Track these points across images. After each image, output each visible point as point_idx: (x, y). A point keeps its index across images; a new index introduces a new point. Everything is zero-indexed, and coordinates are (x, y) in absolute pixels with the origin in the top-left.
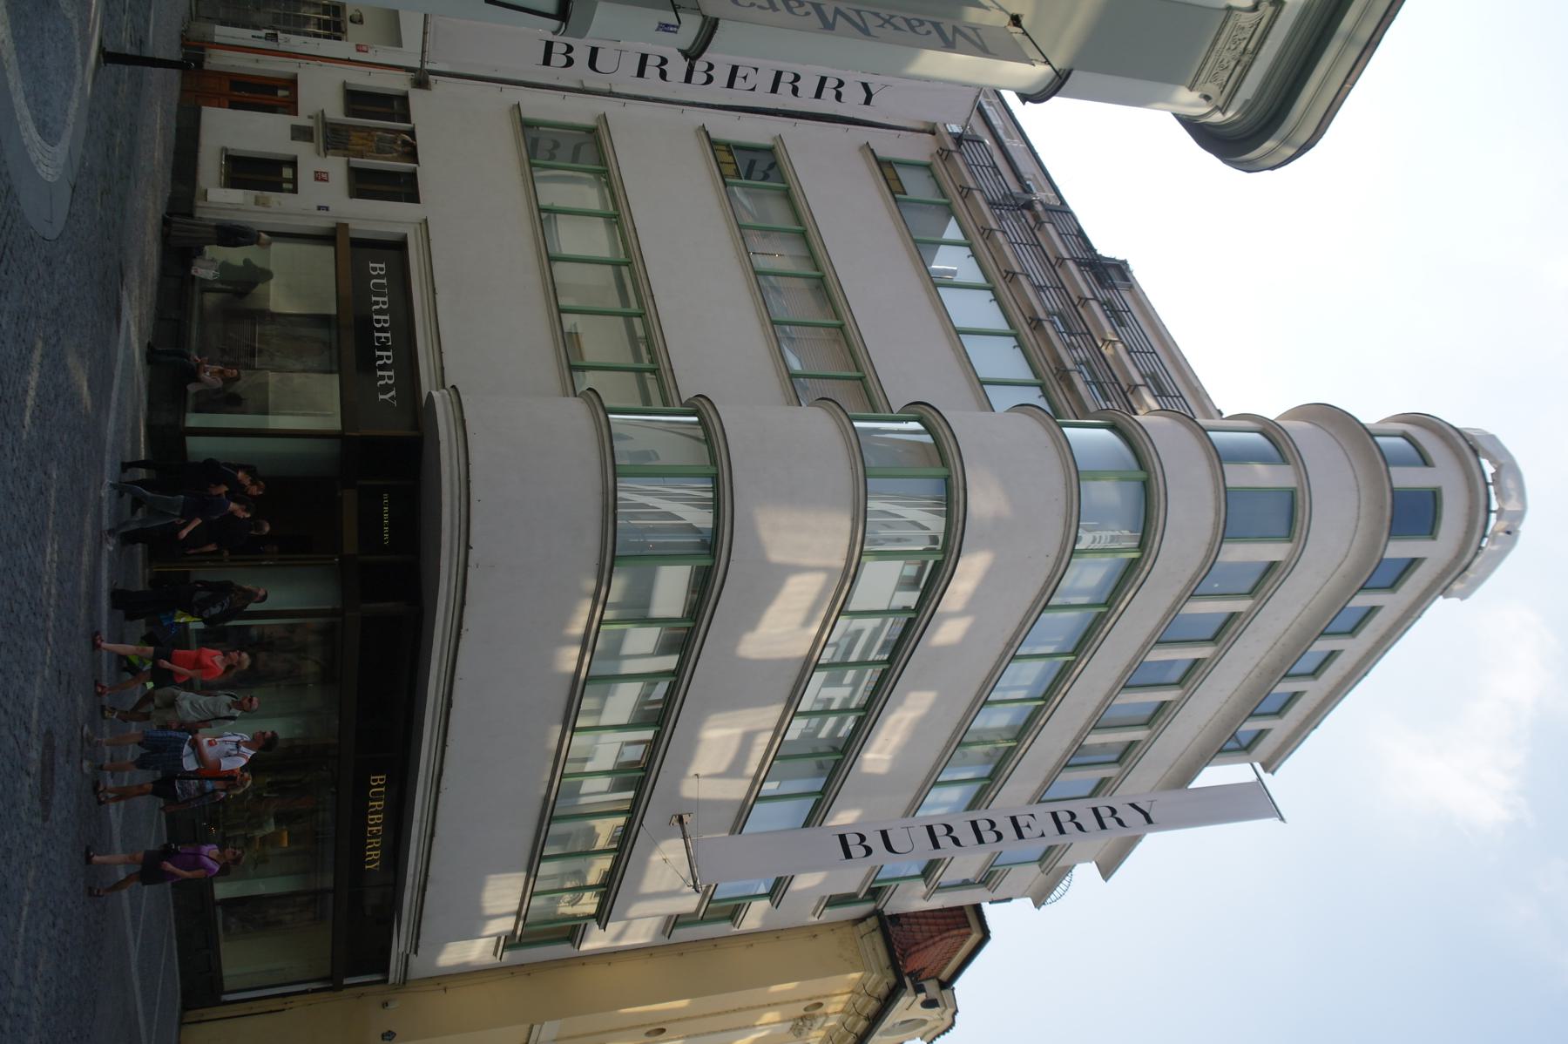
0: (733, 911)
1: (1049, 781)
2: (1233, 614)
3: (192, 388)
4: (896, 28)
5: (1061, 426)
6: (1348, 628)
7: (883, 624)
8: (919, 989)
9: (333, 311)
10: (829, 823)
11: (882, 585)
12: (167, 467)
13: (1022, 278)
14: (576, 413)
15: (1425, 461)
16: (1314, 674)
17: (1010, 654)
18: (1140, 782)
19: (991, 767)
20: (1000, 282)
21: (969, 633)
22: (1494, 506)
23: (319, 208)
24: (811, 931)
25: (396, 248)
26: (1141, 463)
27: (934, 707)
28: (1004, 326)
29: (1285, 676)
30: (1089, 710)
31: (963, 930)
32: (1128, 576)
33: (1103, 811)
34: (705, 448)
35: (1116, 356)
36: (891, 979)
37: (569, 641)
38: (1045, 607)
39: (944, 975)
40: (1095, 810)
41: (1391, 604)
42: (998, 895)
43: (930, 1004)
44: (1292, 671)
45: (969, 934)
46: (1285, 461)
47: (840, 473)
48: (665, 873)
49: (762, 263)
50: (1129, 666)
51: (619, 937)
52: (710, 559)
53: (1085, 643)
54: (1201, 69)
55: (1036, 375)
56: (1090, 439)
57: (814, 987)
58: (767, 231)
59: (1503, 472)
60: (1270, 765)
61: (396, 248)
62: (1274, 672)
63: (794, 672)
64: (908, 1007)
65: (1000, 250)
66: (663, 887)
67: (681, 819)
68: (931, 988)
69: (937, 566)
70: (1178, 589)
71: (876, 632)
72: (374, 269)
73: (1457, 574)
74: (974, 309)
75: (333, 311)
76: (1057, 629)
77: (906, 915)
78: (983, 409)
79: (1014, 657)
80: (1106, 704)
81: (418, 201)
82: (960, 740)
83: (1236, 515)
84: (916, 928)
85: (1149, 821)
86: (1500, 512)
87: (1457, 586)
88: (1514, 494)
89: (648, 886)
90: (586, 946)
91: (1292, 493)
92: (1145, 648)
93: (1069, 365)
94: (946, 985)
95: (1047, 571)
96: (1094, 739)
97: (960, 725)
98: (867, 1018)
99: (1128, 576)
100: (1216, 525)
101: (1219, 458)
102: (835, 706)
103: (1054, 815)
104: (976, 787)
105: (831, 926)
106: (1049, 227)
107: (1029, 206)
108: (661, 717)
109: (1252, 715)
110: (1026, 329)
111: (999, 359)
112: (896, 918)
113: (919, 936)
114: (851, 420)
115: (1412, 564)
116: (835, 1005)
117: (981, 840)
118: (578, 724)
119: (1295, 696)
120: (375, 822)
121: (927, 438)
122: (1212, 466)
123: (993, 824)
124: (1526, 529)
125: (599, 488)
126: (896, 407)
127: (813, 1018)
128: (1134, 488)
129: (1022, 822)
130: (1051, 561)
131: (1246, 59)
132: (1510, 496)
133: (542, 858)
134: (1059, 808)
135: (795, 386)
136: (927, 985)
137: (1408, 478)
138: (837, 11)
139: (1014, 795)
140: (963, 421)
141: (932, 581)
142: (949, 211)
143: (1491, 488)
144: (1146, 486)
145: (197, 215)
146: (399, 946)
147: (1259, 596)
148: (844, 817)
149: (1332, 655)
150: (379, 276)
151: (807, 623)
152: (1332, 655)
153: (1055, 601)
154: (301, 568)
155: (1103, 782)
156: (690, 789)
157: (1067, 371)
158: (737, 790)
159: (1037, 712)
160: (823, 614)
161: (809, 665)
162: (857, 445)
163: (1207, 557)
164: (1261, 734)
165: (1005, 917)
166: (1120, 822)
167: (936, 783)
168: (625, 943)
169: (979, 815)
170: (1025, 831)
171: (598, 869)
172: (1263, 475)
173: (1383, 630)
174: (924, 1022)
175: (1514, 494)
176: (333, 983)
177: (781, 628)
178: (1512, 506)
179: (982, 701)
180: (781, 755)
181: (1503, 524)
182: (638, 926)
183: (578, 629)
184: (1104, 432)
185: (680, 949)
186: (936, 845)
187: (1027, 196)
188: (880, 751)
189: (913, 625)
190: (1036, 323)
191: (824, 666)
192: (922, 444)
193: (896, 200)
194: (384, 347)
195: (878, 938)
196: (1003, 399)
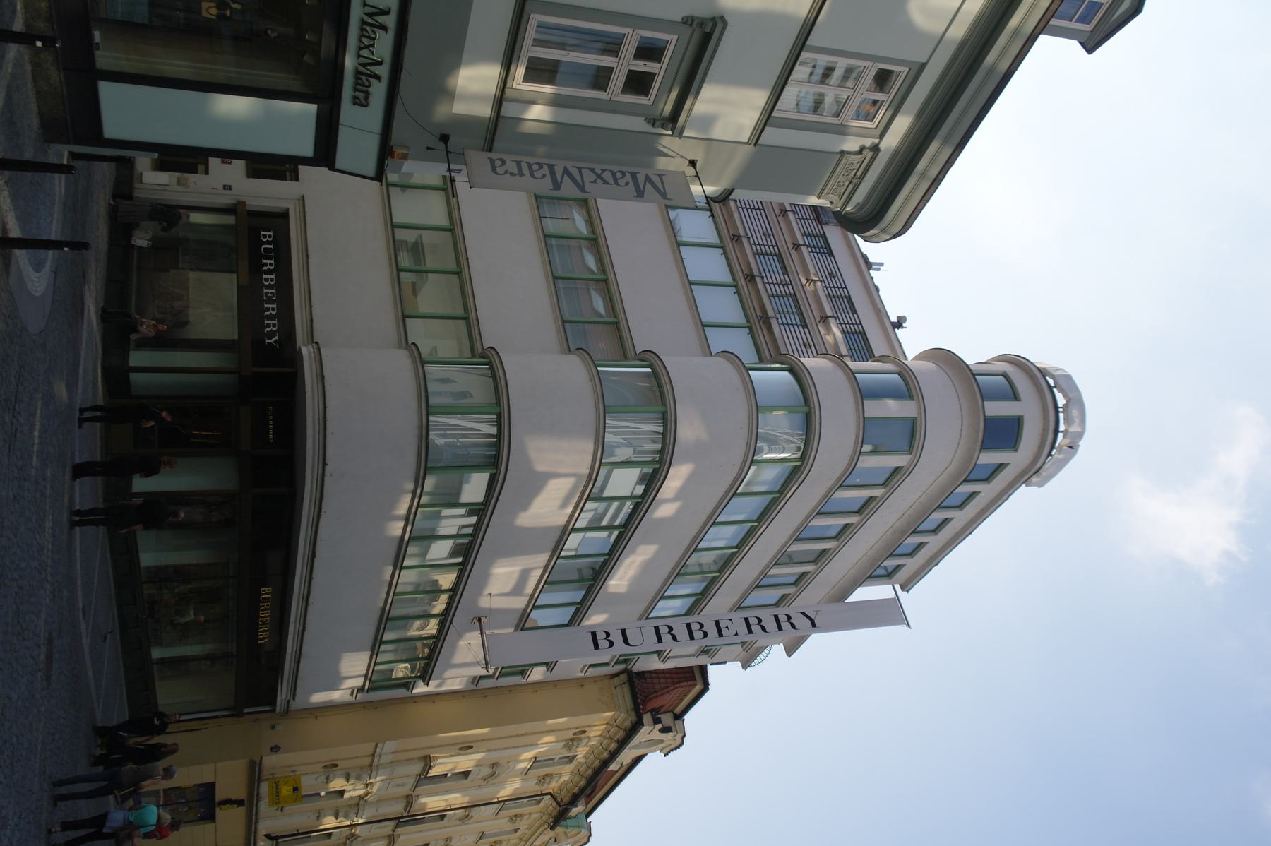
0: (523, 671)
1: (745, 596)
3: (133, 337)
4: (605, 182)
7: (610, 536)
8: (657, 721)
9: (236, 337)
10: (586, 623)
12: (120, 406)
14: (402, 359)
17: (712, 521)
18: (809, 598)
19: (704, 584)
21: (679, 511)
22: (1062, 427)
23: (225, 187)
24: (580, 683)
25: (279, 219)
26: (807, 401)
27: (657, 554)
31: (693, 681)
32: (794, 475)
33: (783, 619)
35: (815, 292)
36: (633, 717)
37: (397, 518)
39: (678, 710)
40: (776, 617)
41: (986, 491)
42: (715, 659)
43: (666, 730)
45: (694, 685)
48: (466, 658)
49: (551, 226)
51: (440, 685)
52: (495, 458)
53: (765, 515)
54: (826, 184)
55: (748, 321)
56: (773, 380)
57: (580, 721)
60: (906, 587)
61: (279, 219)
63: (557, 534)
64: (648, 732)
65: (731, 215)
66: (468, 660)
67: (480, 620)
68: (667, 719)
72: (265, 236)
73: (1033, 473)
75: (236, 337)
76: (743, 509)
77: (650, 672)
80: (764, 574)
81: (297, 180)
82: (679, 572)
83: (871, 434)
84: (656, 681)
85: (814, 625)
86: (1065, 433)
87: (1034, 479)
88: (1077, 420)
89: (458, 658)
90: (416, 691)
91: (914, 421)
92: (809, 518)
93: (770, 313)
94: (679, 717)
98: (617, 742)
99: (794, 475)
103: (747, 620)
104: (693, 599)
105: (595, 679)
108: (467, 552)
109: (890, 555)
111: (722, 306)
112: (641, 674)
113: (657, 687)
114: (596, 366)
116: (596, 732)
117: (692, 637)
118: (385, 638)
120: (265, 615)
122: (856, 403)
123: (702, 626)
124: (1083, 444)
125: (416, 423)
127: (580, 740)
128: (799, 418)
129: (722, 625)
130: (736, 469)
131: (855, 181)
132: (1073, 422)
133: (382, 642)
134: (751, 615)
136: (662, 716)
137: (996, 409)
138: (566, 171)
139: (719, 605)
141: (653, 481)
143: (1061, 415)
144: (808, 418)
145: (136, 194)
146: (282, 695)
148: (596, 619)
150: (268, 243)
154: (210, 481)
155: (784, 597)
156: (484, 602)
158: (520, 603)
160: (575, 501)
161: (567, 530)
163: (849, 465)
165: (724, 676)
166: (793, 626)
167: (662, 598)
168: (444, 688)
169: (691, 619)
170: (724, 631)
171: (440, 606)
172: (893, 408)
173: (982, 505)
174: (662, 741)
175: (1077, 420)
176: (236, 711)
177: (547, 507)
178: (1074, 429)
180: (550, 581)
181: (1067, 441)
182: (452, 679)
183: (402, 510)
184: (787, 373)
185: (485, 693)
186: (660, 641)
188: (621, 579)
189: (641, 504)
194: (270, 301)
195: (626, 688)
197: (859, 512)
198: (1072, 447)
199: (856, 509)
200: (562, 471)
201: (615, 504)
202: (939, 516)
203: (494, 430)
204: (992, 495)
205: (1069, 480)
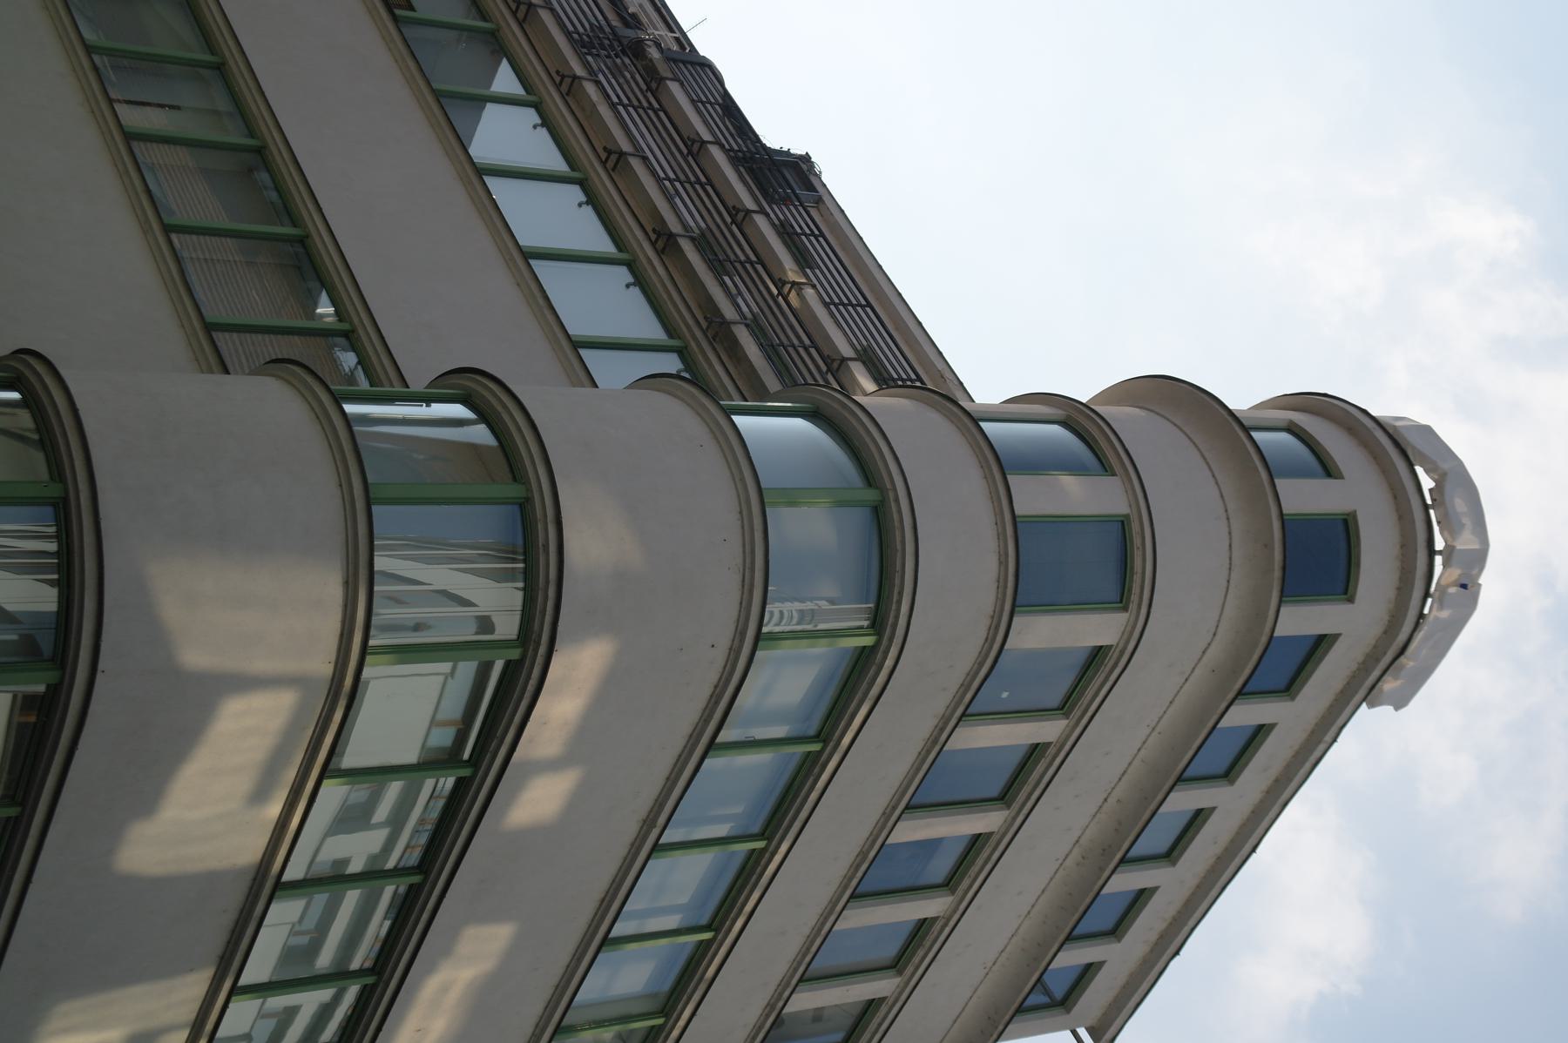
2: (1035, 748)
5: (728, 412)
6: (1221, 769)
7: (337, 999)
11: (405, 712)
13: (635, 163)
15: (1328, 469)
16: (1171, 855)
17: (650, 843)
20: (595, 170)
21: (575, 804)
22: (1439, 544)
28: (605, 246)
29: (1123, 861)
30: (791, 947)
32: (856, 681)
34: (39, 457)
38: (712, 746)
41: (1288, 718)
44: (1133, 853)
46: (1106, 468)
47: (318, 494)
49: (134, 118)
50: (862, 854)
53: (783, 812)
56: (778, 433)
58: (155, 63)
59: (1448, 487)
62: (1106, 852)
63: (233, 899)
69: (512, 671)
70: (940, 703)
71: (325, 1012)
73: (1392, 663)
74: (552, 216)
76: (735, 785)
78: (576, 383)
79: (657, 848)
80: (822, 933)
83: (1037, 565)
86: (1448, 553)
87: (1389, 685)
91: (1123, 523)
92: (888, 820)
95: (713, 676)
96: (805, 1001)
97: (560, 989)
99: (856, 681)
100: (1001, 582)
101: (999, 465)
102: (355, 867)
106: (674, 87)
107: (636, 50)
109: (1070, 938)
110: (646, 251)
111: (603, 302)
115: (1320, 644)
119: (1140, 897)
121: (480, 434)
122: (988, 477)
124: (1488, 580)
126: (418, 384)
128: (858, 519)
130: (720, 655)
135: (214, 342)
137: (1305, 497)
140: (547, 401)
142: (498, 48)
147: (1077, 713)
149: (1198, 818)
151: (260, 795)
152: (1198, 818)
153: (724, 737)
157: (725, 324)
159: (700, 954)
160: (291, 774)
161: (264, 884)
162: (349, 445)
163: (989, 641)
164: (1088, 972)
175: (1466, 520)
178: (1466, 542)
179: (600, 939)
181: (1455, 573)
187: (630, 33)
190: (665, 242)
191: (296, 885)
192: (474, 448)
193: (395, 19)
196: (614, 371)
197: (896, 965)
198: (1468, 587)
199: (995, 793)
200: (261, 665)
201: (394, 788)
202: (1072, 958)
203: (52, 547)
204: (1191, 882)
205: (1468, 672)
